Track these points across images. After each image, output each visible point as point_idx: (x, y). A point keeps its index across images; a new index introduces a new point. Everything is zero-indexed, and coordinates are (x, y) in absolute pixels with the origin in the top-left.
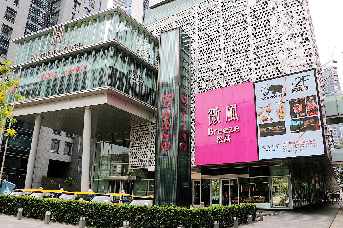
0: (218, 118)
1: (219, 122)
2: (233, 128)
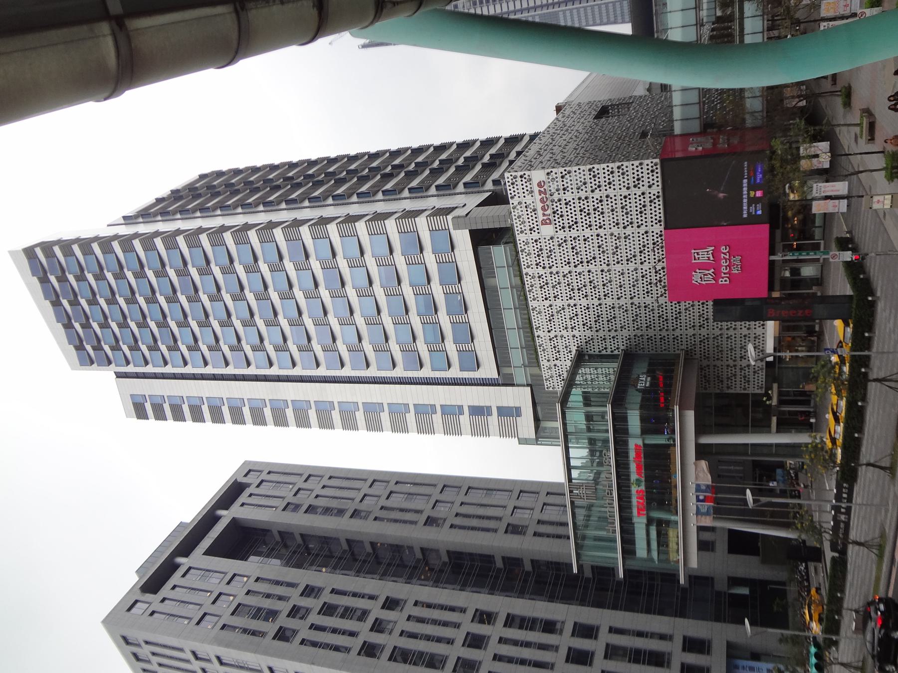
0: (707, 272)
1: (713, 270)
2: (725, 254)
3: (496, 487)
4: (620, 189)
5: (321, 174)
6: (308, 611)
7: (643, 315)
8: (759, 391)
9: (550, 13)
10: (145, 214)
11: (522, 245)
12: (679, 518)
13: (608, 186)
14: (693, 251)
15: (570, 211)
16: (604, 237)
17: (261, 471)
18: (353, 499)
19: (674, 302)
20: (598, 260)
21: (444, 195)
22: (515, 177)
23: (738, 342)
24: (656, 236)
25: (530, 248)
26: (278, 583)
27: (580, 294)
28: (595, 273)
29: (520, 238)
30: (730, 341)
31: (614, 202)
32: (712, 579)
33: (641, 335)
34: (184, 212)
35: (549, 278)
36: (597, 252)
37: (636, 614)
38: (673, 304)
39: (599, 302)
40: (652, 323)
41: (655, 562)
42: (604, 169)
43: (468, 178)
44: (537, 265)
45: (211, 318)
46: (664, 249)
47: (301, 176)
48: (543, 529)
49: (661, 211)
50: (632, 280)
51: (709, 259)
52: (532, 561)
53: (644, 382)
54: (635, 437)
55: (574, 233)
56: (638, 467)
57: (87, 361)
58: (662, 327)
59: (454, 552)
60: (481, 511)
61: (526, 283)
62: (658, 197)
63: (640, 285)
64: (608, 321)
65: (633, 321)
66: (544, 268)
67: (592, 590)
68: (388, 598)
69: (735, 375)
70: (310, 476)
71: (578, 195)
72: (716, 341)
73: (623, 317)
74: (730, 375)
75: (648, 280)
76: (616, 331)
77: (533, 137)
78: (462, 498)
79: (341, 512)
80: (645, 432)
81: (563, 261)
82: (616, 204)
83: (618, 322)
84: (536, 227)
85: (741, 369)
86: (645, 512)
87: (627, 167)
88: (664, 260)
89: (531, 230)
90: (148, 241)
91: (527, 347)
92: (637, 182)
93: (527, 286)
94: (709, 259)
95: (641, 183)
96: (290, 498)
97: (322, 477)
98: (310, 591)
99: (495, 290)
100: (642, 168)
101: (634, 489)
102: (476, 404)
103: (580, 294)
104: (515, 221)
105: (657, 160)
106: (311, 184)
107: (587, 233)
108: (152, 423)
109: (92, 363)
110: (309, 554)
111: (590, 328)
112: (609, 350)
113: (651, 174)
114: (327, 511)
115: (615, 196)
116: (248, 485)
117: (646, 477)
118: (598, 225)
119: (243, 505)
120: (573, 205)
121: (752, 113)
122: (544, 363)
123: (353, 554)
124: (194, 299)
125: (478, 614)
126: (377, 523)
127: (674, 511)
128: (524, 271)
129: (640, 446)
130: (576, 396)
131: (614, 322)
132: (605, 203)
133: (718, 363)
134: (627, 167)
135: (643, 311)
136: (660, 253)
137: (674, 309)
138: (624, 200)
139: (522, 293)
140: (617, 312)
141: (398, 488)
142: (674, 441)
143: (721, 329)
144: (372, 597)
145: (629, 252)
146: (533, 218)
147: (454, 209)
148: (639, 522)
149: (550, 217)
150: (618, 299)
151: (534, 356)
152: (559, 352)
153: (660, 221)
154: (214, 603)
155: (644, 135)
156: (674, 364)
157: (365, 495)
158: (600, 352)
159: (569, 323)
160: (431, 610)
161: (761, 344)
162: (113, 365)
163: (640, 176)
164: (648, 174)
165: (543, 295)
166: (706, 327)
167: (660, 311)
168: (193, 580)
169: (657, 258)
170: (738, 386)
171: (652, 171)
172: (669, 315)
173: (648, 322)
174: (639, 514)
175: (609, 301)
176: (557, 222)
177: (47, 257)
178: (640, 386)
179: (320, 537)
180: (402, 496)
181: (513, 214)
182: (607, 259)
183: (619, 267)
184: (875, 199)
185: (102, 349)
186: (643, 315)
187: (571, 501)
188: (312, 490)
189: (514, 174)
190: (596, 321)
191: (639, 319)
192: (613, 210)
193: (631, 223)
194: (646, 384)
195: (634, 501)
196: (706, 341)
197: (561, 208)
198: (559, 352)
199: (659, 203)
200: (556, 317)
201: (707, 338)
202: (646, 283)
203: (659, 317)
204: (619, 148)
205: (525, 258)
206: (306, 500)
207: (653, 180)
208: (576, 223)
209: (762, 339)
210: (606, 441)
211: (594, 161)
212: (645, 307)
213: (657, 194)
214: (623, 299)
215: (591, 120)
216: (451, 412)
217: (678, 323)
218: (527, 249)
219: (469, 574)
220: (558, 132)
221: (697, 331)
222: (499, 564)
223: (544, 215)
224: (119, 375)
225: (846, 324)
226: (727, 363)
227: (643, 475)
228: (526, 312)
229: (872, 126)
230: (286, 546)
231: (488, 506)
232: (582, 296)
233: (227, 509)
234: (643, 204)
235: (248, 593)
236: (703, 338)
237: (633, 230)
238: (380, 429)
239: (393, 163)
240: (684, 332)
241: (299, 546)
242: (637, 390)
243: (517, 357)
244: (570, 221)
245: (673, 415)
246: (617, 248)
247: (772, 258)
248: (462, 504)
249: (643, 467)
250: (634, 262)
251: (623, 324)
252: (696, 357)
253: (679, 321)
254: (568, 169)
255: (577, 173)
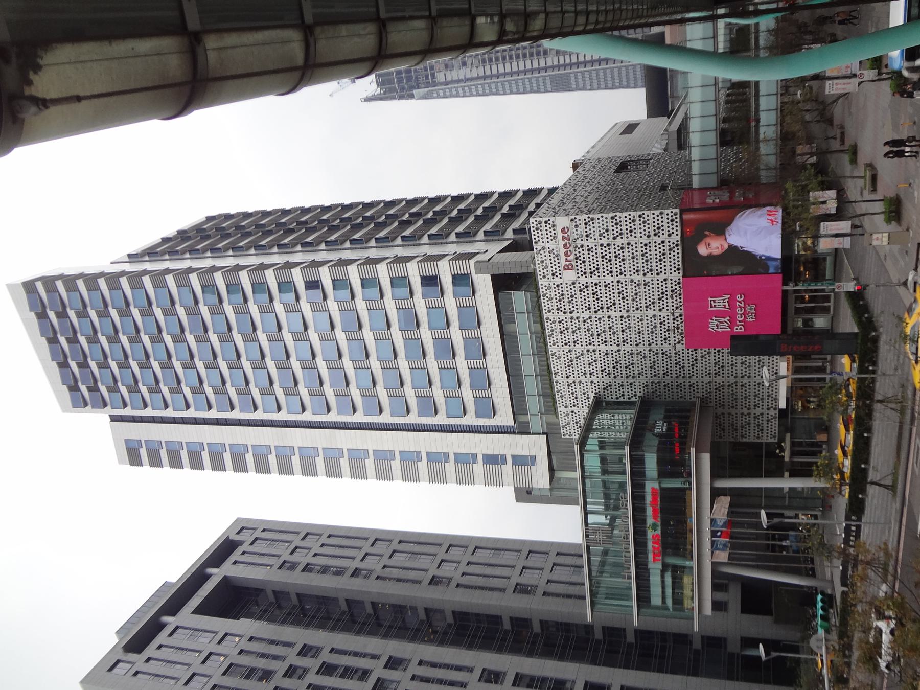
0: (723, 320)
1: (728, 318)
2: (739, 302)
3: (504, 547)
4: (641, 237)
5: (336, 219)
6: (305, 670)
7: (660, 362)
8: (772, 440)
9: (561, 74)
10: (151, 253)
11: (544, 290)
12: (694, 564)
13: (630, 234)
14: (710, 299)
15: (592, 258)
16: (624, 283)
17: (255, 529)
18: (353, 558)
19: (691, 350)
20: (618, 306)
21: (464, 242)
22: (540, 223)
23: (752, 391)
24: (674, 283)
25: (552, 293)
26: (272, 642)
27: (600, 340)
28: (615, 319)
29: (542, 283)
30: (744, 389)
31: (635, 249)
32: (725, 639)
33: (658, 382)
34: (193, 252)
35: (569, 324)
36: (617, 298)
37: (648, 673)
38: (690, 351)
39: (618, 348)
40: (669, 370)
41: (669, 610)
42: (626, 217)
43: (488, 227)
44: (558, 309)
45: (183, 385)
46: (682, 297)
47: (315, 221)
48: (553, 588)
49: (680, 259)
50: (650, 327)
51: (725, 307)
52: (541, 622)
53: (661, 427)
54: (652, 480)
55: (595, 279)
56: (655, 511)
57: (80, 403)
58: (679, 374)
59: (461, 613)
60: (488, 571)
61: (547, 327)
62: (677, 245)
63: (658, 332)
64: (626, 367)
65: (651, 367)
66: (565, 313)
67: (602, 652)
68: (390, 657)
69: (749, 424)
70: (307, 534)
71: (600, 242)
72: (731, 389)
73: (641, 364)
74: (744, 424)
75: (666, 327)
76: (633, 377)
77: (552, 191)
78: (468, 557)
79: (339, 572)
80: (662, 474)
81: (583, 307)
82: (637, 251)
83: (636, 369)
84: (559, 272)
85: (755, 417)
86: (660, 558)
87: (648, 216)
88: (682, 307)
89: (553, 275)
90: (158, 278)
91: (544, 395)
92: (657, 231)
93: (547, 331)
94: (725, 307)
95: (661, 232)
96: (286, 556)
97: (320, 535)
98: (305, 651)
99: (514, 336)
100: (662, 218)
101: (650, 534)
102: (491, 452)
103: (600, 340)
104: (537, 266)
105: (677, 210)
106: (326, 229)
107: (608, 279)
108: (146, 470)
109: (86, 404)
110: (305, 616)
111: (609, 374)
112: (626, 397)
113: (671, 223)
114: (325, 570)
115: (636, 243)
116: (240, 543)
117: (661, 519)
118: (619, 271)
119: (235, 563)
120: (595, 252)
121: (768, 169)
122: (561, 409)
123: (352, 615)
124: (202, 339)
125: (486, 673)
126: (379, 582)
127: (689, 556)
128: (545, 316)
129: (656, 490)
130: (593, 442)
131: (632, 369)
132: (626, 250)
133: (733, 411)
134: (648, 216)
135: (660, 358)
136: (678, 301)
137: (691, 357)
138: (644, 248)
139: (542, 340)
140: (635, 358)
141: (402, 547)
142: (690, 484)
143: (736, 377)
144: (374, 657)
145: (648, 299)
146: (556, 263)
147: (474, 254)
148: (655, 567)
149: (573, 263)
150: (637, 345)
151: (552, 404)
152: (576, 398)
153: (678, 269)
154: (204, 662)
155: (664, 188)
156: (689, 411)
157: (367, 554)
158: (617, 398)
159: (587, 369)
160: (437, 670)
161: (774, 392)
162: (109, 407)
163: (660, 225)
164: (668, 223)
165: (563, 341)
166: (722, 375)
167: (677, 358)
168: (180, 639)
169: (675, 306)
170: (752, 435)
171: (672, 221)
172: (686, 362)
173: (665, 369)
174: (654, 560)
175: (627, 347)
176: (579, 268)
177: (47, 291)
178: (658, 430)
179: (317, 597)
180: (406, 555)
181: (536, 258)
182: (626, 305)
183: (638, 314)
184: (875, 236)
185: (98, 390)
186: (660, 362)
187: (587, 546)
188: (310, 549)
189: (538, 219)
190: (614, 367)
191: (657, 365)
192: (633, 258)
193: (651, 270)
194: (662, 429)
195: (650, 546)
196: (721, 389)
197: (607, 222)
198: (576, 398)
199: (678, 252)
200: (574, 362)
201: (722, 386)
202: (664, 330)
203: (676, 364)
204: (640, 199)
205: (547, 303)
206: (302, 558)
207: (673, 229)
208: (598, 269)
209: (775, 387)
210: (622, 485)
211: (616, 210)
212: (663, 353)
213: (676, 243)
214: (641, 345)
215: (612, 174)
216: (465, 460)
217: (694, 370)
218: (549, 294)
219: (474, 636)
220: (580, 183)
221: (712, 379)
222: (507, 625)
223: (567, 260)
224: (114, 419)
225: (853, 361)
226: (741, 411)
227: (659, 519)
228: (545, 359)
229: (874, 178)
230: (280, 607)
231: (496, 566)
232: (601, 342)
233: (218, 567)
234: (662, 252)
235: (241, 652)
236: (718, 386)
237: (652, 277)
238: (390, 478)
239: (411, 211)
240: (700, 379)
241: (294, 607)
242: (654, 435)
243: (534, 404)
244: (592, 267)
245: (690, 457)
246: (636, 294)
247: (785, 288)
248: (469, 563)
249: (659, 511)
250: (653, 308)
251: (641, 371)
252: (712, 404)
253: (695, 368)
254: (591, 216)
255: (600, 221)
